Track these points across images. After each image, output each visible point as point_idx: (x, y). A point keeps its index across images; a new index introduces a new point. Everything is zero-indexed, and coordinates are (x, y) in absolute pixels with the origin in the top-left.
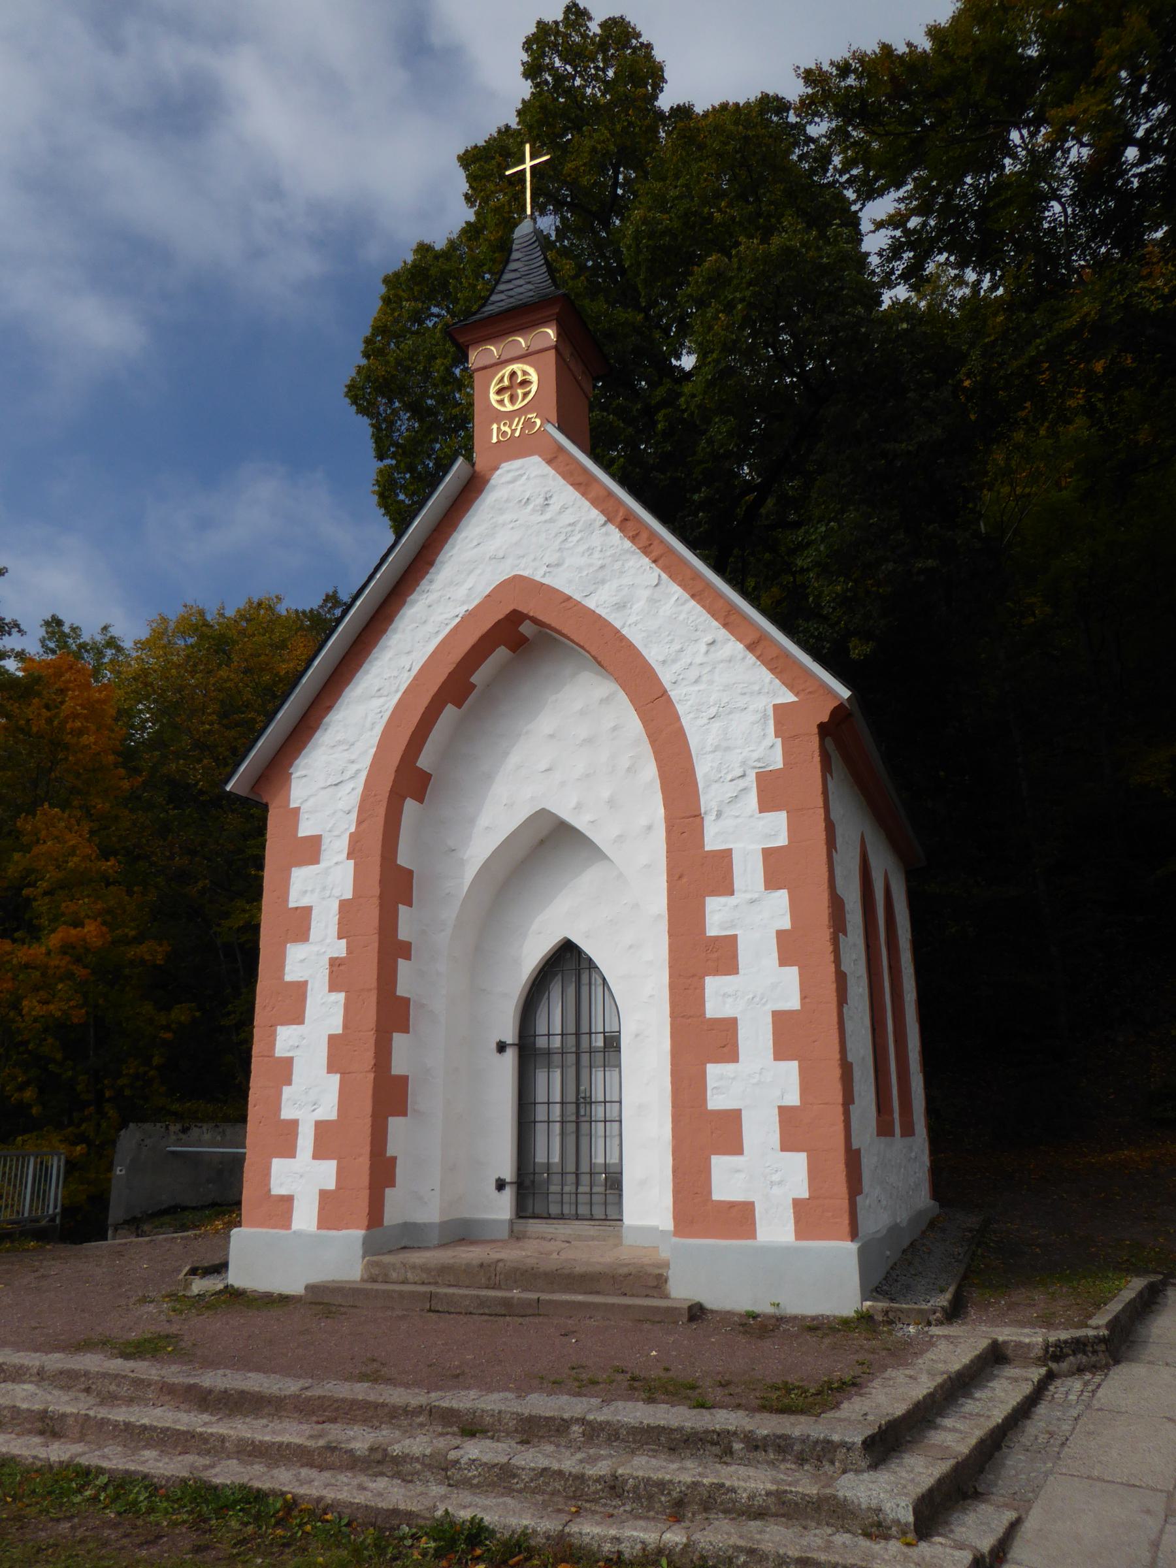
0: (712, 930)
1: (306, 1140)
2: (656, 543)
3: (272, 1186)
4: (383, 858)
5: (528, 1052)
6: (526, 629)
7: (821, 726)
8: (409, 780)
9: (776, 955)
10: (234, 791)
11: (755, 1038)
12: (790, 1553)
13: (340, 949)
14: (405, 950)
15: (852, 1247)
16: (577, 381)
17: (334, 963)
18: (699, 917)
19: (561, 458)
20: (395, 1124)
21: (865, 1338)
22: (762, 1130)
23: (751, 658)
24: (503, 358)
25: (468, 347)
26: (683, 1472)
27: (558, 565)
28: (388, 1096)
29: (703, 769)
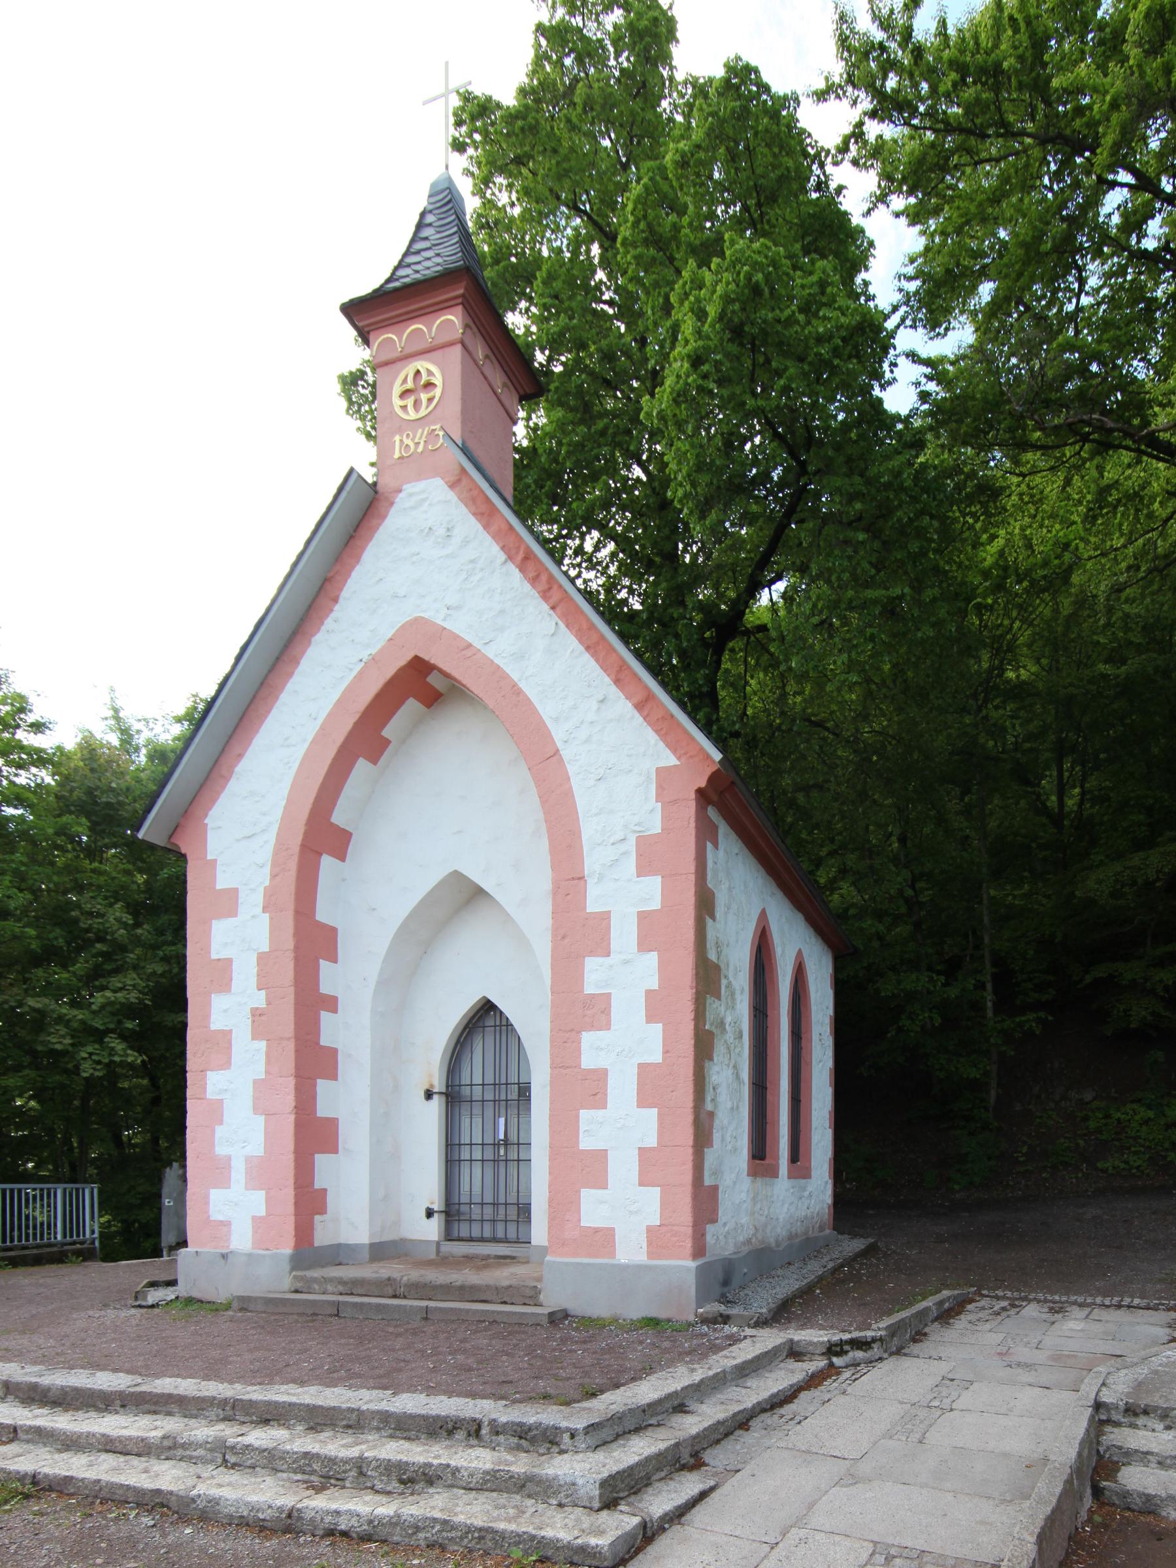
0: (589, 989)
1: (238, 1173)
2: (555, 587)
3: (211, 1212)
4: (297, 913)
5: (453, 1097)
6: (433, 680)
7: (700, 791)
8: (321, 837)
9: (643, 1013)
10: (147, 839)
11: (622, 1087)
12: (476, 1523)
13: (259, 999)
14: (331, 1004)
15: (692, 1264)
16: (495, 393)
17: (256, 1013)
18: (578, 977)
19: (464, 481)
20: (322, 1161)
21: (660, 1337)
22: (623, 1168)
23: (638, 719)
24: (408, 351)
25: (368, 333)
26: (416, 1453)
27: (458, 608)
28: (313, 1135)
29: (589, 830)
